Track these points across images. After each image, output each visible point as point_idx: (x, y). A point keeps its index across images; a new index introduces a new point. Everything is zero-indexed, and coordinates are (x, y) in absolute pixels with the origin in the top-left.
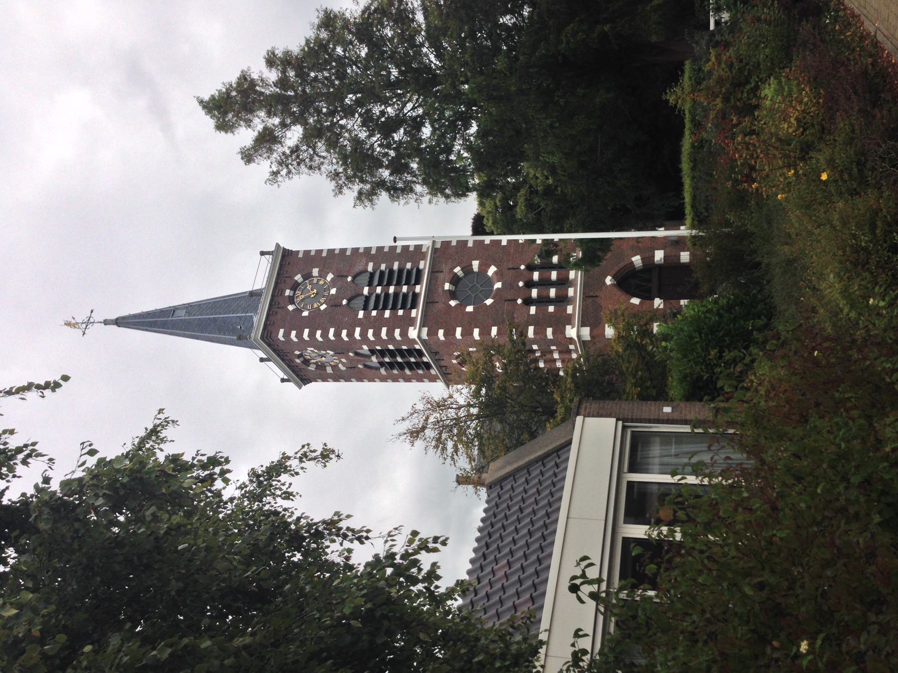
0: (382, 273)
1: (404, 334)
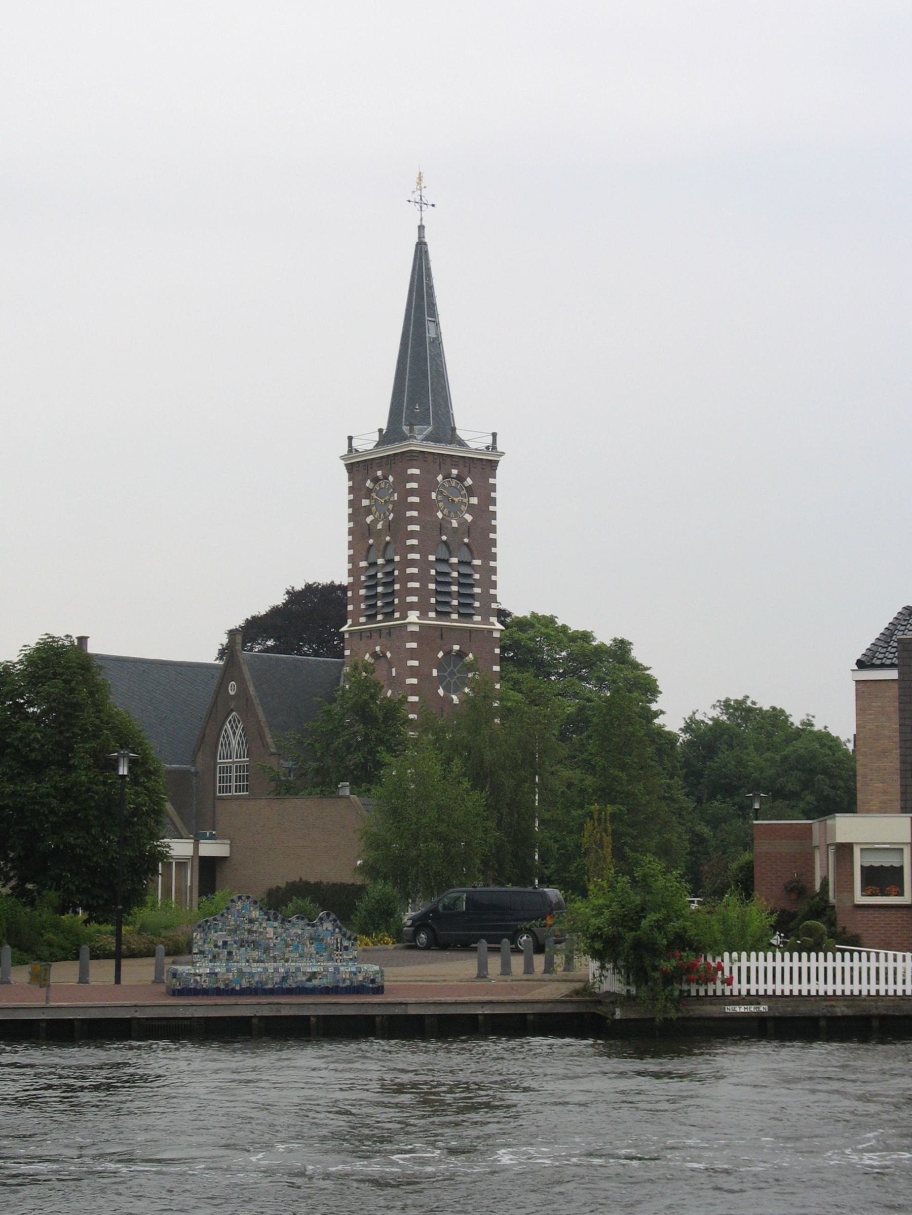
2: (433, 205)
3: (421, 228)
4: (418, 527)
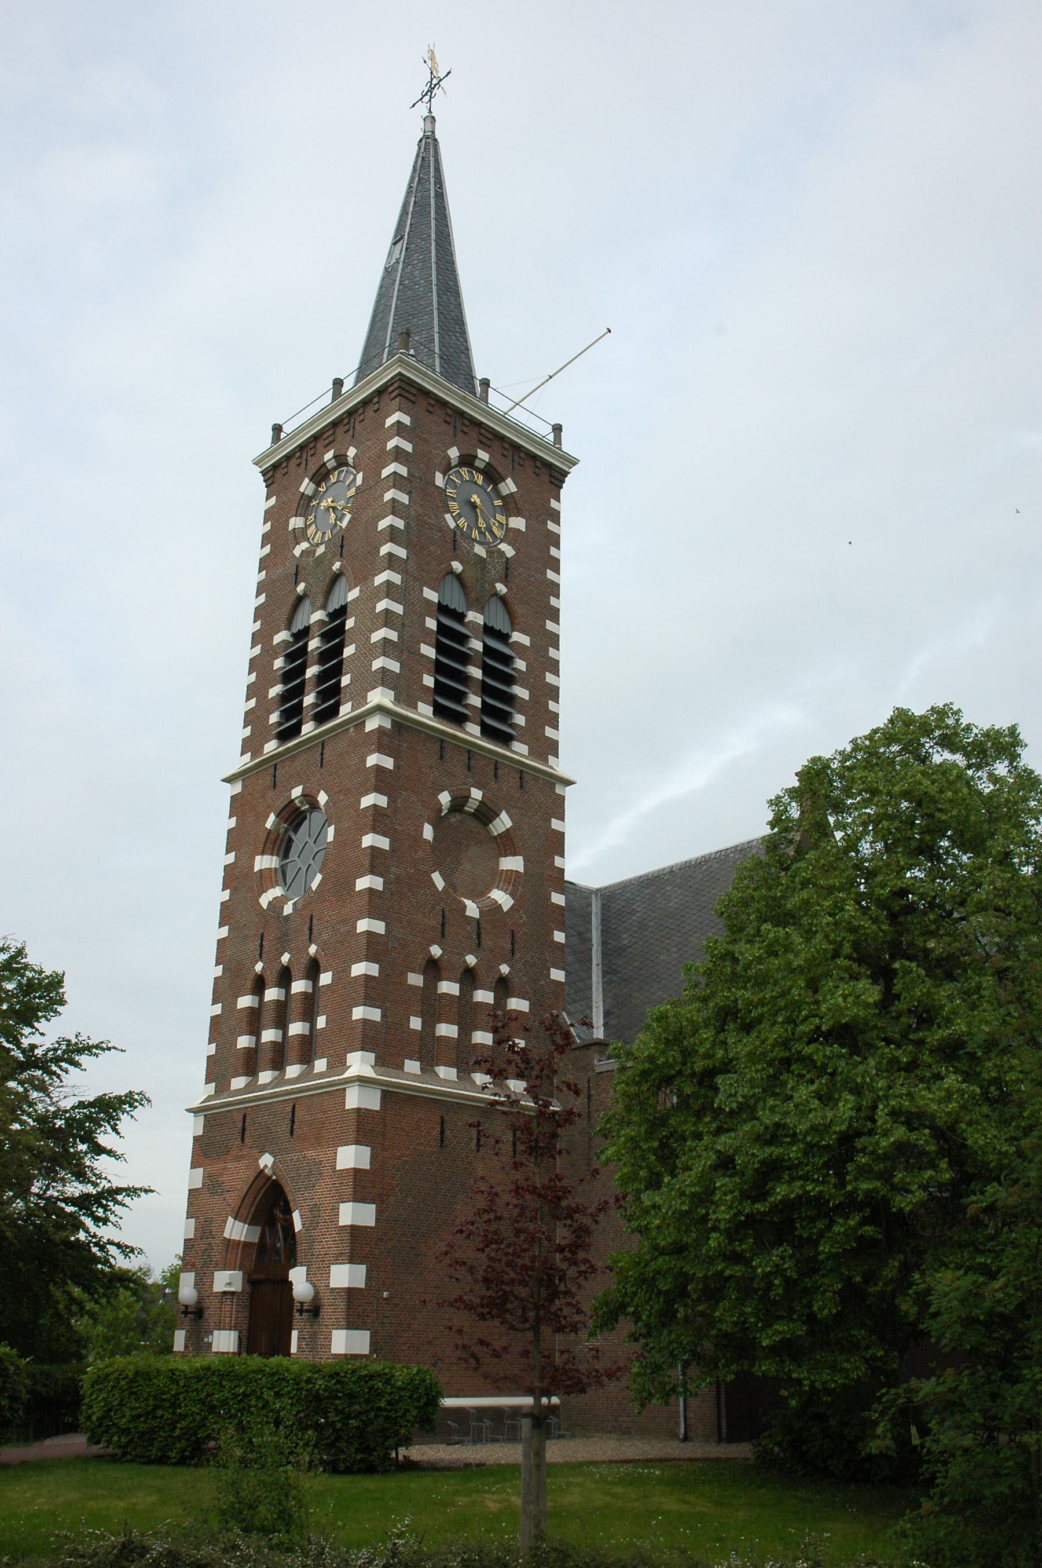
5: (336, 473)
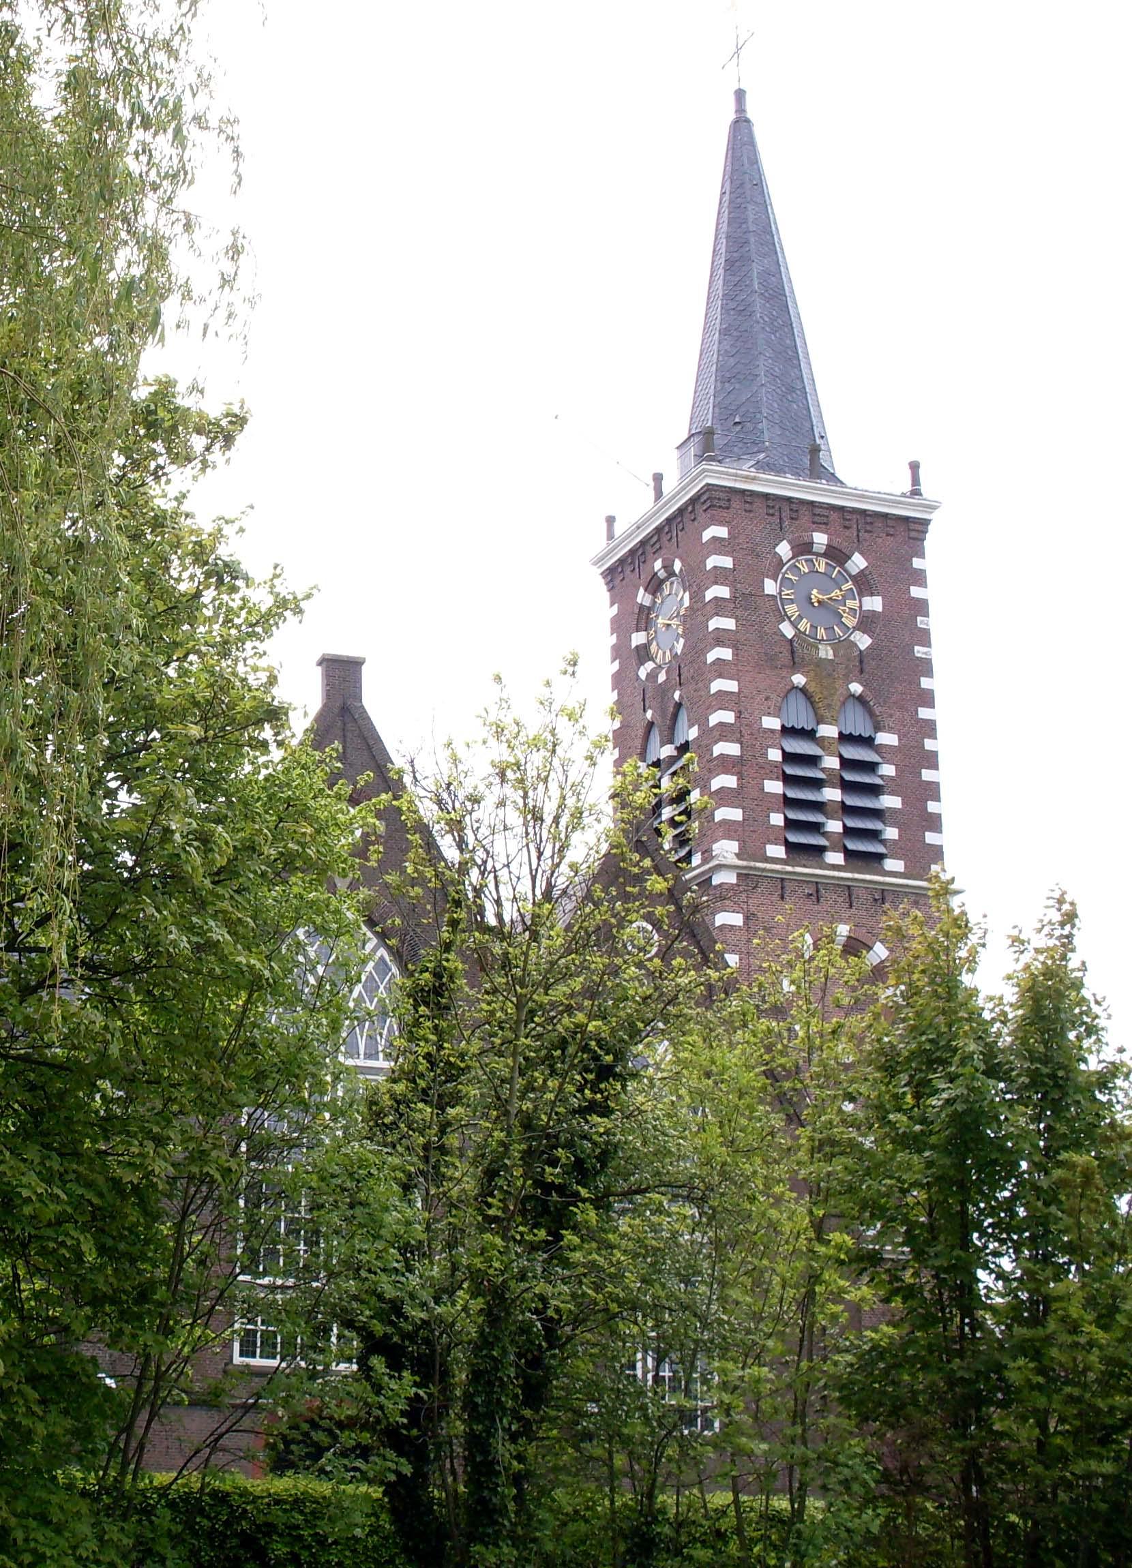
0: (871, 767)
1: (729, 829)
2: (985, 916)
3: (740, 95)
4: (902, 863)
5: (668, 583)
